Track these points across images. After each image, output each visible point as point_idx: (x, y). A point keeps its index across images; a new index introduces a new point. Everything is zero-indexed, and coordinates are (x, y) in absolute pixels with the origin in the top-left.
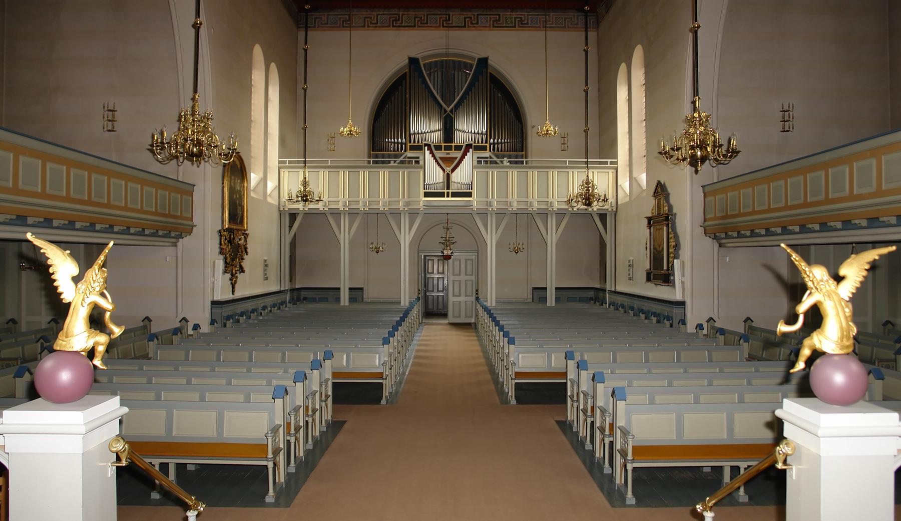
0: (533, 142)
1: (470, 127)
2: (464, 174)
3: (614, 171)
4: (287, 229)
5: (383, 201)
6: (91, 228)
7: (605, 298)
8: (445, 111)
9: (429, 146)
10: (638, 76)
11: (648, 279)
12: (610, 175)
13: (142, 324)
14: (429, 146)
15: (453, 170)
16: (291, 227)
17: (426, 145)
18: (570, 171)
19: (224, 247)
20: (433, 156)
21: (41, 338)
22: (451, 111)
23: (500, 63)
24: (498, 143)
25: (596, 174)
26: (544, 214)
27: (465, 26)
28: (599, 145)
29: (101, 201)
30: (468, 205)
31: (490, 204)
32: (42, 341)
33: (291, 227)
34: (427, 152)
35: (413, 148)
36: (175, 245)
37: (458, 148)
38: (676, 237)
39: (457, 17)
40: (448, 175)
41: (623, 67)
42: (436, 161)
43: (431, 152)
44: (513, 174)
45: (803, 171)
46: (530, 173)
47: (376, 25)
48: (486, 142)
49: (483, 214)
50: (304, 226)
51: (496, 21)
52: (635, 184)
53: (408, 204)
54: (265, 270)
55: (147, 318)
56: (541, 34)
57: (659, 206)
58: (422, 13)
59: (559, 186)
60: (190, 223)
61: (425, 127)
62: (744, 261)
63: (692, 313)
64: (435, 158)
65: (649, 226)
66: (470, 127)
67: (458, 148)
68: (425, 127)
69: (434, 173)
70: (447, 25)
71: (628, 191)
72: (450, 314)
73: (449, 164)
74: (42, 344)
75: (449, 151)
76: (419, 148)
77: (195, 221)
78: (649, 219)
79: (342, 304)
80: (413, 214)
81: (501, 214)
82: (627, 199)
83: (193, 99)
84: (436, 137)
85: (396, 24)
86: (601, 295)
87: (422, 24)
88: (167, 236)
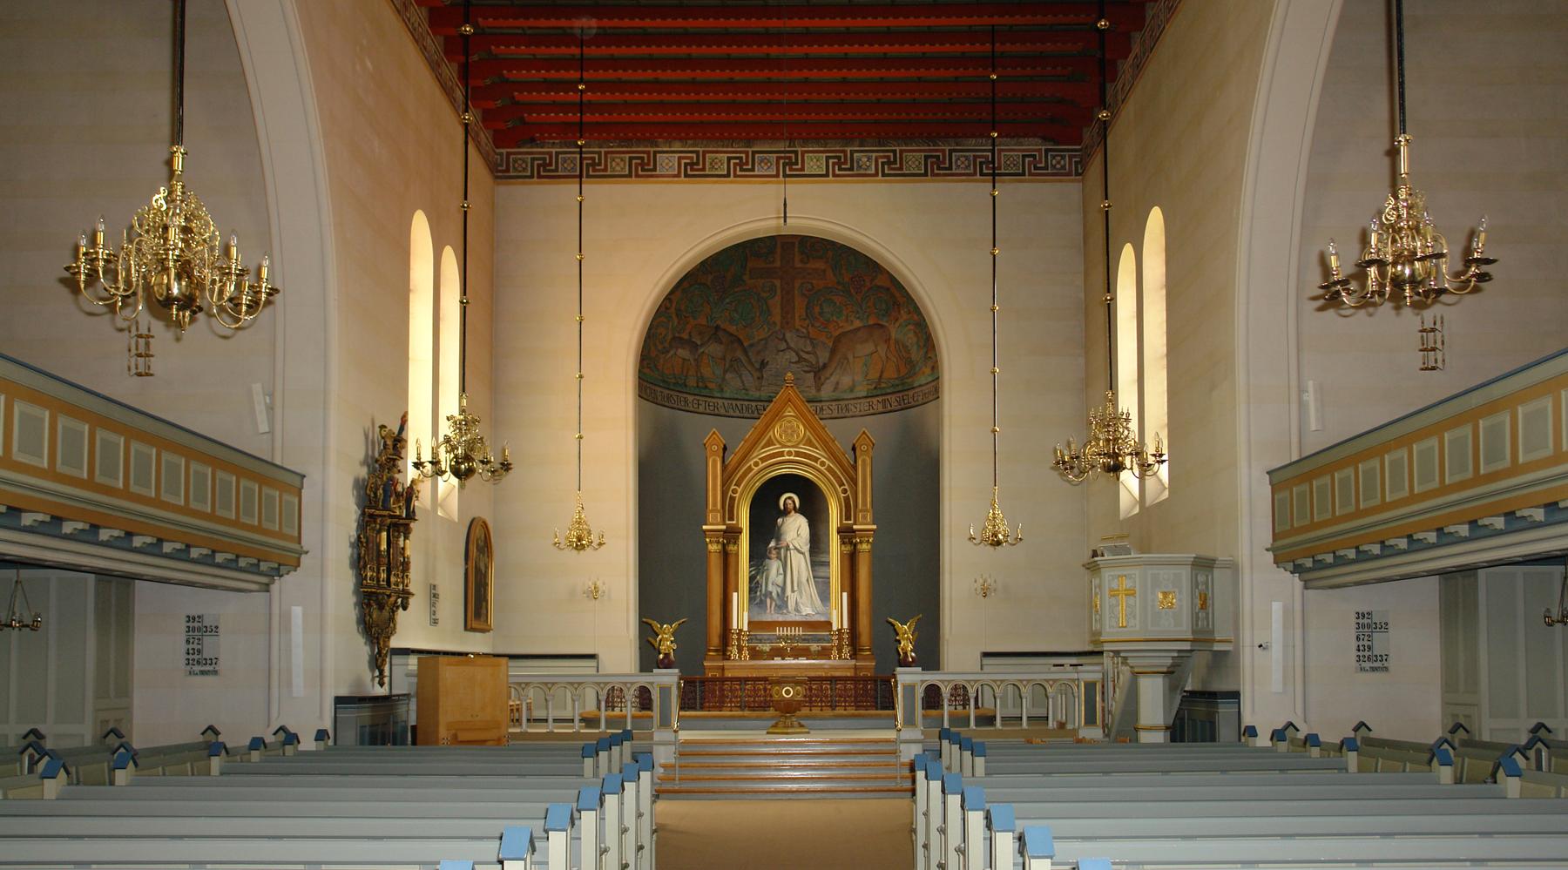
6: (124, 543)
13: (201, 738)
21: (30, 745)
29: (143, 491)
32: (30, 750)
36: (266, 588)
41: (1128, 251)
45: (1437, 429)
54: (433, 605)
55: (211, 728)
56: (979, 190)
60: (296, 546)
62: (1338, 609)
70: (791, 168)
71: (1136, 493)
74: (31, 757)
77: (307, 541)
82: (1137, 510)
83: (272, 395)
87: (743, 169)
88: (254, 569)
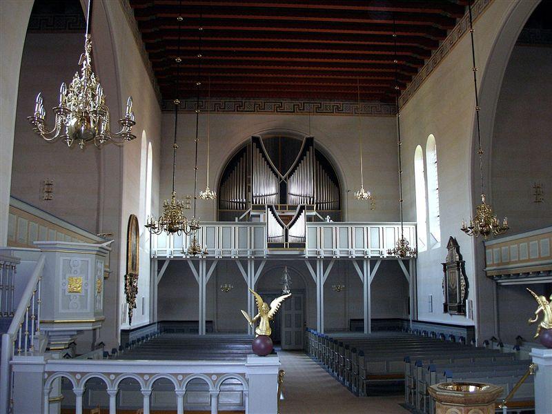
0: (348, 204)
1: (299, 189)
2: (299, 229)
3: (414, 227)
4: (156, 273)
5: (234, 252)
7: (409, 326)
8: (281, 179)
9: (270, 207)
10: (432, 156)
11: (446, 311)
12: (411, 229)
14: (270, 207)
15: (290, 227)
16: (159, 272)
17: (268, 206)
18: (365, 227)
19: (128, 288)
20: (275, 215)
22: (286, 179)
23: (322, 141)
24: (323, 203)
25: (354, 229)
26: (360, 261)
27: (294, 112)
28: (397, 208)
30: (300, 256)
31: (318, 253)
33: (159, 272)
34: (270, 212)
35: (255, 208)
37: (293, 208)
38: (466, 279)
39: (288, 104)
40: (287, 231)
41: (419, 148)
42: (277, 219)
43: (273, 213)
44: (398, 226)
46: (217, 228)
47: (224, 110)
48: (313, 203)
49: (313, 261)
50: (173, 272)
51: (318, 108)
52: (432, 238)
53: (254, 253)
57: (451, 255)
58: (260, 101)
59: (382, 240)
61: (266, 190)
63: (479, 334)
64: (276, 217)
65: (445, 270)
66: (299, 189)
67: (293, 208)
68: (266, 190)
69: (275, 229)
71: (426, 242)
72: (283, 342)
73: (287, 222)
75: (285, 211)
76: (261, 208)
78: (445, 265)
79: (200, 334)
80: (258, 261)
81: (327, 261)
84: (273, 199)
85: (240, 109)
86: (406, 324)
87: (260, 109)
